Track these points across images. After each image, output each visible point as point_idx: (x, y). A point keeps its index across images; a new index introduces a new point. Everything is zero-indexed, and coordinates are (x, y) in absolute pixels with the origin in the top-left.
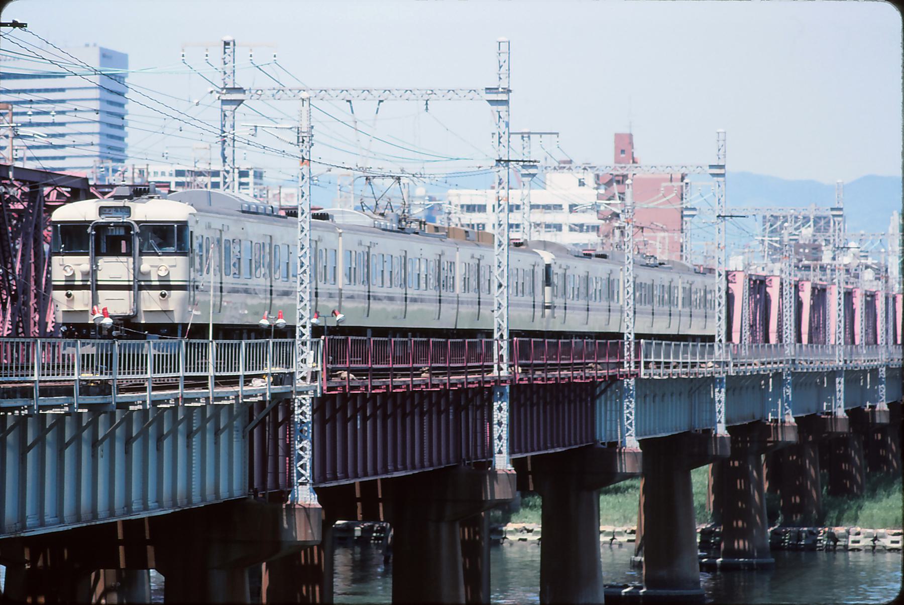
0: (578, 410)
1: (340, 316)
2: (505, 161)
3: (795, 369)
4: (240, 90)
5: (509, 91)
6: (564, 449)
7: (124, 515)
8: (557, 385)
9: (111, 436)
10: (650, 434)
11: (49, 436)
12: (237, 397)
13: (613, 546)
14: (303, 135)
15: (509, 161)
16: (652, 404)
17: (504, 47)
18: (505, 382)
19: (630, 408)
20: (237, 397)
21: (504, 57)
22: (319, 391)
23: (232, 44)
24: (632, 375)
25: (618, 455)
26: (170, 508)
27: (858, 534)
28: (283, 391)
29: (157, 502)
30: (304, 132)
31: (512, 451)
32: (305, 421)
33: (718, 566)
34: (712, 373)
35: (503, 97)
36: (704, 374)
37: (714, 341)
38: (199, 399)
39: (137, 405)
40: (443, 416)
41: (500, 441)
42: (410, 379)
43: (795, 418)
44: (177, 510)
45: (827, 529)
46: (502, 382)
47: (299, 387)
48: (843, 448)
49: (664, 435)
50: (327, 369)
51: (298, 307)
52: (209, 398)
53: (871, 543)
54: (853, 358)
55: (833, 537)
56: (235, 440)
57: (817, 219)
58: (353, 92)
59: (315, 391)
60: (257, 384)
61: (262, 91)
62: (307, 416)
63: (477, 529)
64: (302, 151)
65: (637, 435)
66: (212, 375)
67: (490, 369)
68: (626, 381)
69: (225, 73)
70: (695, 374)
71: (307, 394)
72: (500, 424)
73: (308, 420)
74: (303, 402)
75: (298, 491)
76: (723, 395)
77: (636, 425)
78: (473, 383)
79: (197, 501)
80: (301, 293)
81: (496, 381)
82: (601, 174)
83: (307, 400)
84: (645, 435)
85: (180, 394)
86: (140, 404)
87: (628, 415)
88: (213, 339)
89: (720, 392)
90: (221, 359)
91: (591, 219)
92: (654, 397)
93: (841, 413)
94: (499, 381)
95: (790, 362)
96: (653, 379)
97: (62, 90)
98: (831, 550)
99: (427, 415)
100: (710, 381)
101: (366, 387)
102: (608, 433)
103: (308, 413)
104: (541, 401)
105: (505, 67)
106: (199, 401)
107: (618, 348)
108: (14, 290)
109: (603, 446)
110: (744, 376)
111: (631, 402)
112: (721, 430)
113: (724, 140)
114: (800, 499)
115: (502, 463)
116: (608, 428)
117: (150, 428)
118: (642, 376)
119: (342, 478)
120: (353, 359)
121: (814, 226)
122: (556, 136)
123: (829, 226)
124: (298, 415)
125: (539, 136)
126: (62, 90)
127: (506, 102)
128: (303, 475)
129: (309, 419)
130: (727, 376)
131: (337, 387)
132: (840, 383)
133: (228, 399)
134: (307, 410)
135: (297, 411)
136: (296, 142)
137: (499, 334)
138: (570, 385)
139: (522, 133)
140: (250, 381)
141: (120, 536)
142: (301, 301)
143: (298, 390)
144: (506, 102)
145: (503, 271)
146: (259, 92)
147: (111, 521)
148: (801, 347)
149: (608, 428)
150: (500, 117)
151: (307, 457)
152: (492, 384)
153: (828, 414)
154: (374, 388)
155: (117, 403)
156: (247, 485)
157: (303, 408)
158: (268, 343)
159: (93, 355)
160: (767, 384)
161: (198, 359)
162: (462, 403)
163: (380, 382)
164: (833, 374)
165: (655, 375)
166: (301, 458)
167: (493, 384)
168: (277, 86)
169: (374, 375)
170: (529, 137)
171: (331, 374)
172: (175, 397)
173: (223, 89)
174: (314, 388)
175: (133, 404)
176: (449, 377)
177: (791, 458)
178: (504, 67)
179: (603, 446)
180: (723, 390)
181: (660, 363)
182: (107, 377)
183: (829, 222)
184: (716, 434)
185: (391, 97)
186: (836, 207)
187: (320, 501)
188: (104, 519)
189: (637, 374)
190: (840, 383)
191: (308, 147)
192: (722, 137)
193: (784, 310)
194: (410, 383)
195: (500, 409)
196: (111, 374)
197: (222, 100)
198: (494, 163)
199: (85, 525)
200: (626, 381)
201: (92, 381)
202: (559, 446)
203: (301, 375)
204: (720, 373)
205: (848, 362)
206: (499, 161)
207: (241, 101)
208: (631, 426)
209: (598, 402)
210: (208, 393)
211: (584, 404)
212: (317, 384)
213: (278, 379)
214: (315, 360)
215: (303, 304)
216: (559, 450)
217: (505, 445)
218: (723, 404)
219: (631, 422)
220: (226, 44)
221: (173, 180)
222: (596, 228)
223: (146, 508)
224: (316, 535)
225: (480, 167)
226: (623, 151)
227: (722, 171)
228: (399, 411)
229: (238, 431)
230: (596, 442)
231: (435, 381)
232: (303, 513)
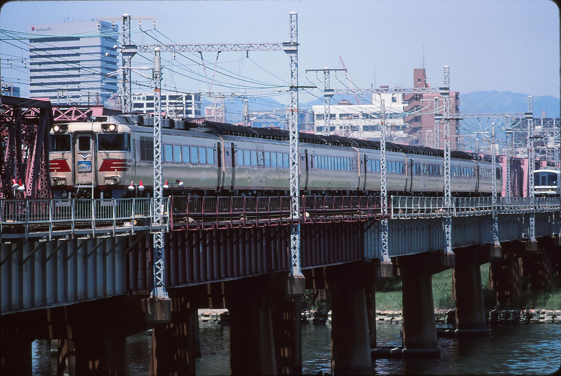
0: (400, 240)
1: (181, 184)
2: (295, 87)
3: (500, 212)
4: (134, 47)
5: (297, 44)
6: (342, 263)
7: (42, 306)
8: (333, 224)
9: (32, 257)
10: (402, 254)
11: (79, 251)
12: (112, 233)
13: (393, 323)
14: (156, 73)
15: (298, 87)
16: (410, 234)
17: (294, 17)
18: (297, 222)
19: (385, 237)
20: (112, 233)
21: (294, 23)
22: (168, 229)
23: (128, 18)
24: (386, 217)
25: (381, 265)
26: (72, 301)
27: (544, 313)
28: (144, 229)
29: (64, 298)
30: (157, 72)
31: (302, 266)
32: (160, 247)
33: (456, 334)
34: (441, 215)
35: (294, 48)
36: (436, 216)
37: (492, 196)
38: (86, 235)
39: (43, 239)
40: (258, 244)
41: (295, 259)
42: (230, 221)
43: (500, 243)
44: (77, 303)
45: (525, 311)
46: (295, 222)
47: (154, 227)
48: (539, 261)
49: (411, 254)
50: (174, 216)
51: (155, 178)
52: (92, 234)
53: (552, 319)
54: (541, 205)
55: (530, 316)
56: (116, 260)
57: (545, 120)
58: (202, 47)
59: (166, 229)
60: (127, 225)
61: (147, 47)
62: (161, 245)
63: (294, 313)
64: (156, 83)
65: (389, 255)
66: (94, 220)
67: (288, 215)
68: (382, 221)
69: (124, 36)
70: (430, 216)
71: (161, 231)
72: (295, 248)
73: (162, 247)
74: (159, 236)
75: (157, 290)
76: (450, 229)
77: (389, 248)
78: (275, 223)
79: (90, 295)
80: (156, 170)
81: (290, 222)
82: (406, 93)
83: (161, 234)
84: (399, 254)
85: (72, 232)
86: (45, 238)
87: (384, 242)
88: (94, 198)
89: (448, 227)
90: (105, 211)
91: (400, 122)
92: (405, 230)
93: (533, 239)
94: (294, 221)
95: (496, 208)
96: (431, 219)
97: (78, 48)
98: (528, 322)
99: (247, 243)
100: (440, 221)
101: (201, 226)
102: (373, 253)
103: (161, 242)
104: (326, 234)
105: (295, 29)
106: (86, 236)
107: (442, 201)
108: (4, 171)
109: (368, 261)
110: (464, 218)
111: (385, 234)
112: (449, 250)
113: (449, 72)
114: (510, 293)
115: (297, 272)
116: (373, 250)
117: (58, 252)
118: (392, 218)
119: (190, 282)
120: (259, 209)
121: (543, 125)
122: (344, 71)
123: (553, 124)
124: (155, 244)
125: (315, 72)
126: (78, 48)
127: (295, 51)
128: (159, 281)
129: (162, 246)
130: (452, 217)
131: (181, 226)
132: (532, 221)
133: (106, 235)
134: (161, 240)
135: (155, 242)
136: (152, 78)
137: (294, 193)
138: (342, 223)
139: (324, 70)
140: (123, 224)
141: (49, 319)
142: (383, 174)
143: (153, 228)
144: (295, 51)
145: (295, 154)
146: (145, 48)
147: (32, 310)
148: (522, 199)
149: (373, 250)
150: (292, 60)
151: (162, 269)
152: (288, 223)
153: (525, 240)
154: (206, 227)
155: (28, 238)
156: (125, 287)
157: (159, 240)
158: (132, 200)
159: (68, 207)
160: (521, 220)
161: (100, 211)
162: (272, 236)
163: (210, 223)
164: (528, 215)
165: (401, 217)
166: (157, 270)
167: (289, 223)
168: (155, 43)
169: (205, 219)
170: (328, 72)
171: (176, 219)
172: (69, 234)
173: (123, 46)
174: (165, 227)
175: (41, 238)
176: (270, 219)
177: (503, 268)
178: (294, 30)
179: (368, 261)
180: (450, 226)
181: (405, 209)
182: (21, 222)
183: (553, 122)
184: (446, 253)
185: (226, 49)
186: (528, 112)
187: (170, 297)
188: (28, 308)
189: (389, 217)
190: (532, 221)
191: (159, 81)
192: (447, 70)
193: (493, 176)
194: (231, 223)
195: (295, 239)
196: (24, 220)
197: (123, 53)
198: (289, 89)
199: (14, 312)
200: (382, 221)
201: (13, 225)
202: (338, 261)
203: (157, 220)
204: (447, 215)
205: (537, 208)
206: (292, 87)
207: (133, 54)
208: (386, 249)
209: (365, 234)
210: (92, 231)
211: (356, 236)
212: (167, 225)
213: (140, 222)
214: (165, 210)
215: (157, 176)
216: (338, 264)
217: (298, 261)
218: (450, 235)
219: (386, 246)
220: (125, 18)
221: (145, 102)
222: (404, 128)
223: (56, 301)
224: (167, 317)
225: (280, 91)
226: (419, 80)
227: (447, 91)
228: (376, 230)
229: (118, 254)
230: (364, 258)
231: (249, 222)
232: (159, 304)
